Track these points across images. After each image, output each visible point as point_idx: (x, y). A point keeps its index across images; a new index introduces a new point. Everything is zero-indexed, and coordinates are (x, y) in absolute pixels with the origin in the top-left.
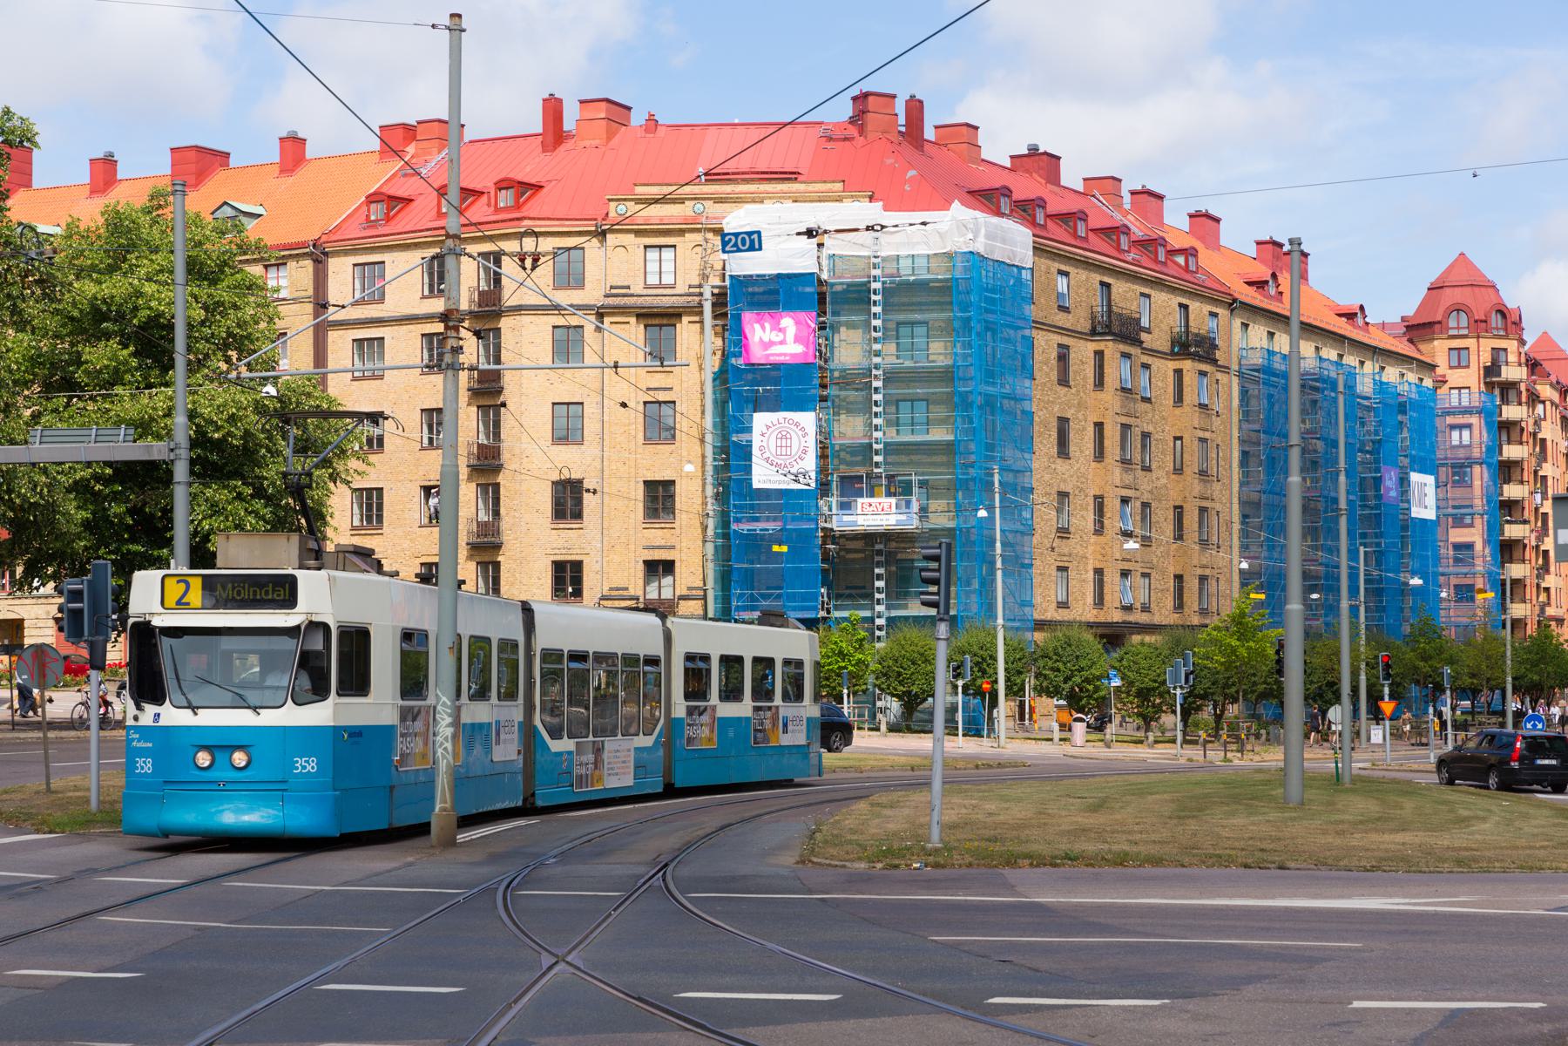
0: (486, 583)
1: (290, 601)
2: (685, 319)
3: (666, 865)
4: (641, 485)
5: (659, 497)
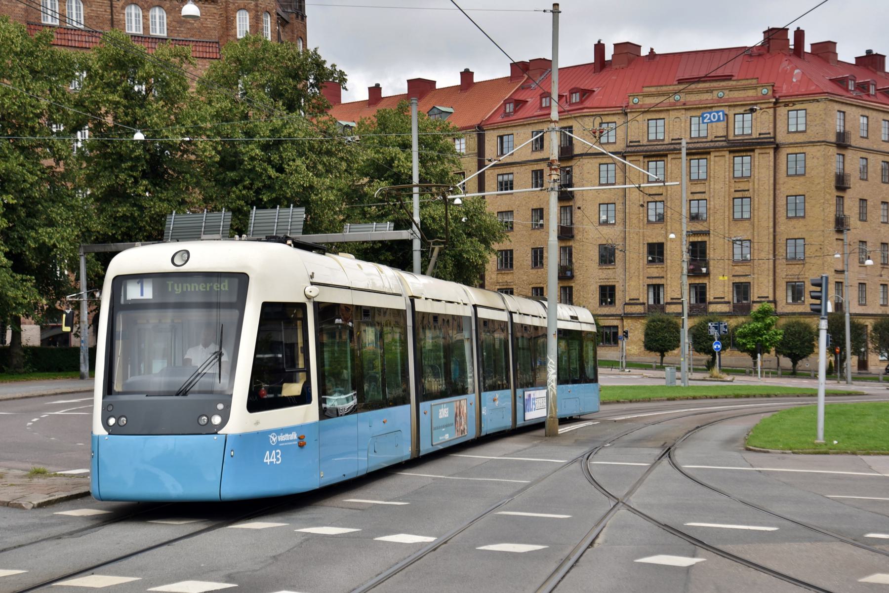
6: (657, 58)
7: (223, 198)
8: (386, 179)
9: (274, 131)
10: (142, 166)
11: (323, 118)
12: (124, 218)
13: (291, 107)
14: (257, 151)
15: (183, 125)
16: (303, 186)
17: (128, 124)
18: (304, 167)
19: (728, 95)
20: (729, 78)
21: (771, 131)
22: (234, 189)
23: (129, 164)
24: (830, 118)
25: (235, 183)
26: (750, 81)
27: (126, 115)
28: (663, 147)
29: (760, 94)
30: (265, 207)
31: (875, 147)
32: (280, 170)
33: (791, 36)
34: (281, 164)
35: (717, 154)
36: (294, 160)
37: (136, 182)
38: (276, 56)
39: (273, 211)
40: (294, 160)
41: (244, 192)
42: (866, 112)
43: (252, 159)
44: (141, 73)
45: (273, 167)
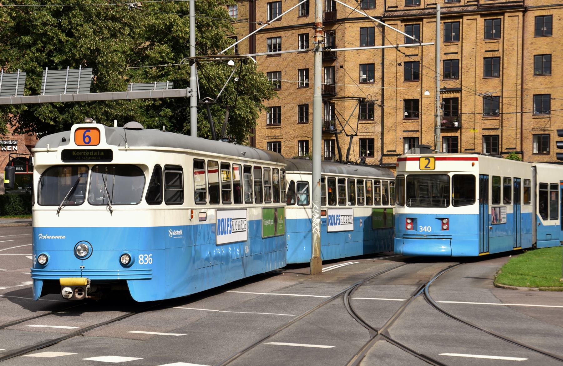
0: (328, 149)
1: (111, 158)
2: (425, 21)
3: (424, 286)
4: (403, 102)
5: (412, 108)
30: (56, 68)
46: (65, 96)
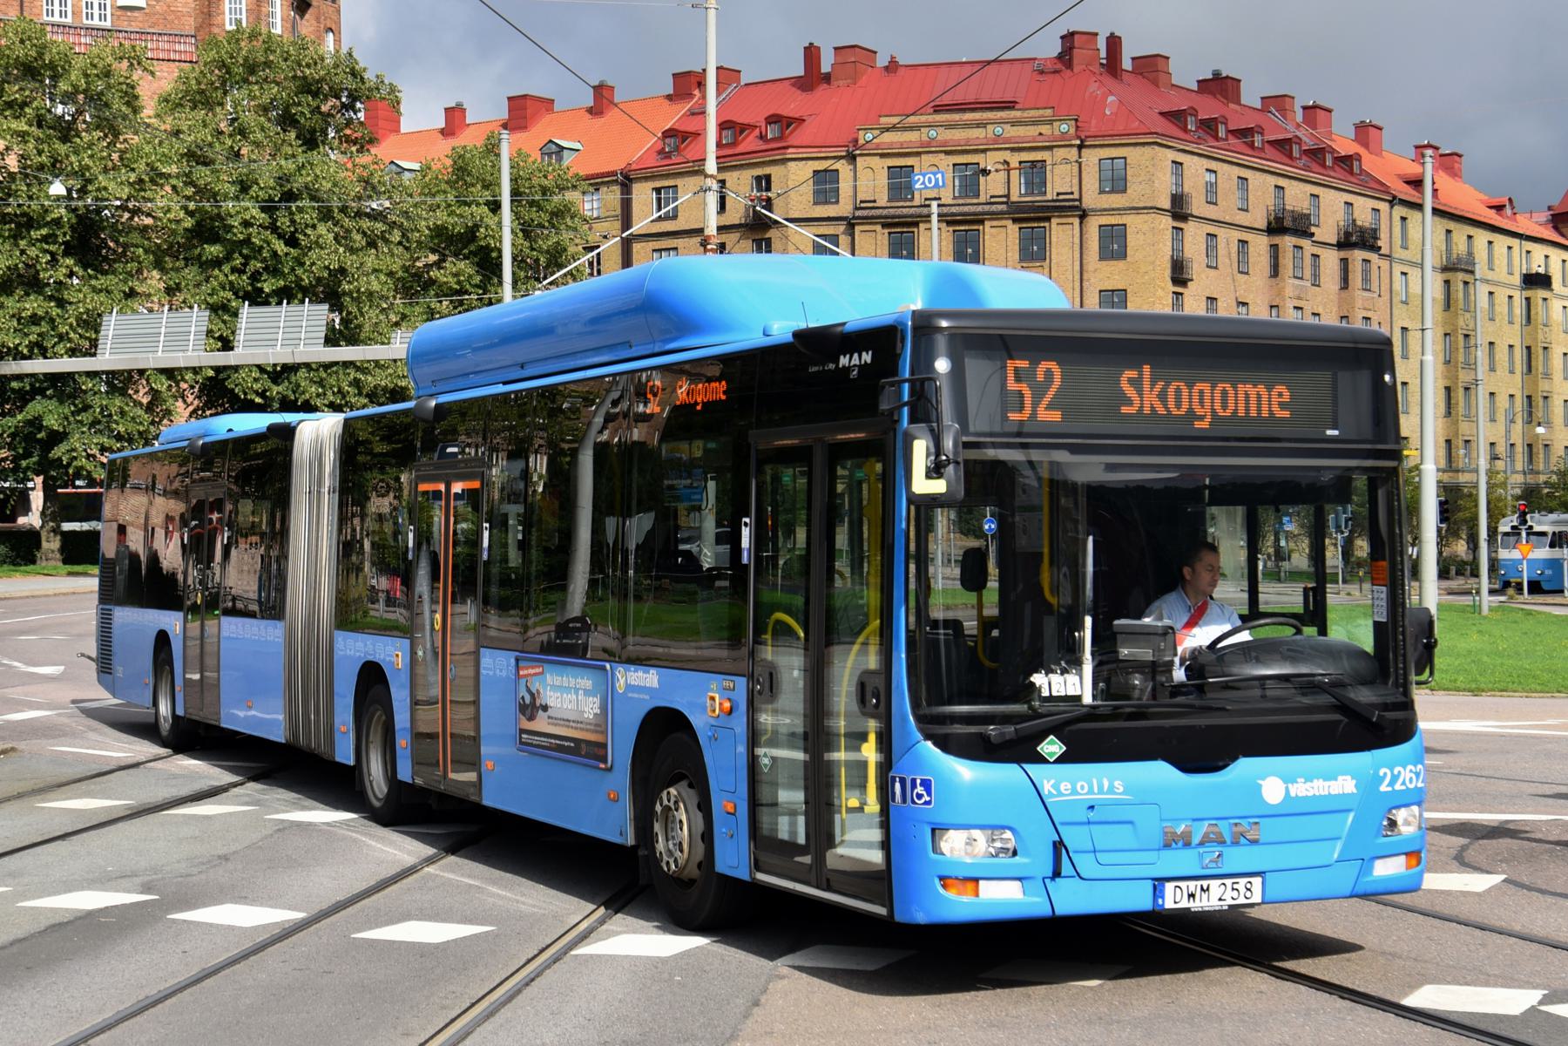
6: (901, 72)
7: (198, 285)
8: (466, 258)
9: (283, 179)
10: (65, 234)
11: (364, 159)
12: (35, 320)
13: (311, 141)
14: (254, 212)
15: (133, 170)
16: (327, 268)
17: (41, 167)
18: (331, 236)
19: (1011, 132)
20: (1009, 105)
21: (1076, 189)
22: (216, 272)
23: (44, 231)
24: (1152, 171)
25: (217, 263)
26: (1041, 112)
27: (40, 153)
28: (912, 211)
29: (1057, 133)
30: (266, 303)
31: (1228, 219)
32: (292, 241)
33: (1102, 44)
34: (293, 233)
35: (995, 223)
36: (314, 227)
37: (54, 261)
38: (286, 60)
39: (278, 309)
40: (314, 227)
41: (232, 278)
42: (1214, 165)
43: (246, 224)
44: (63, 86)
45: (280, 237)
46: (278, 355)
